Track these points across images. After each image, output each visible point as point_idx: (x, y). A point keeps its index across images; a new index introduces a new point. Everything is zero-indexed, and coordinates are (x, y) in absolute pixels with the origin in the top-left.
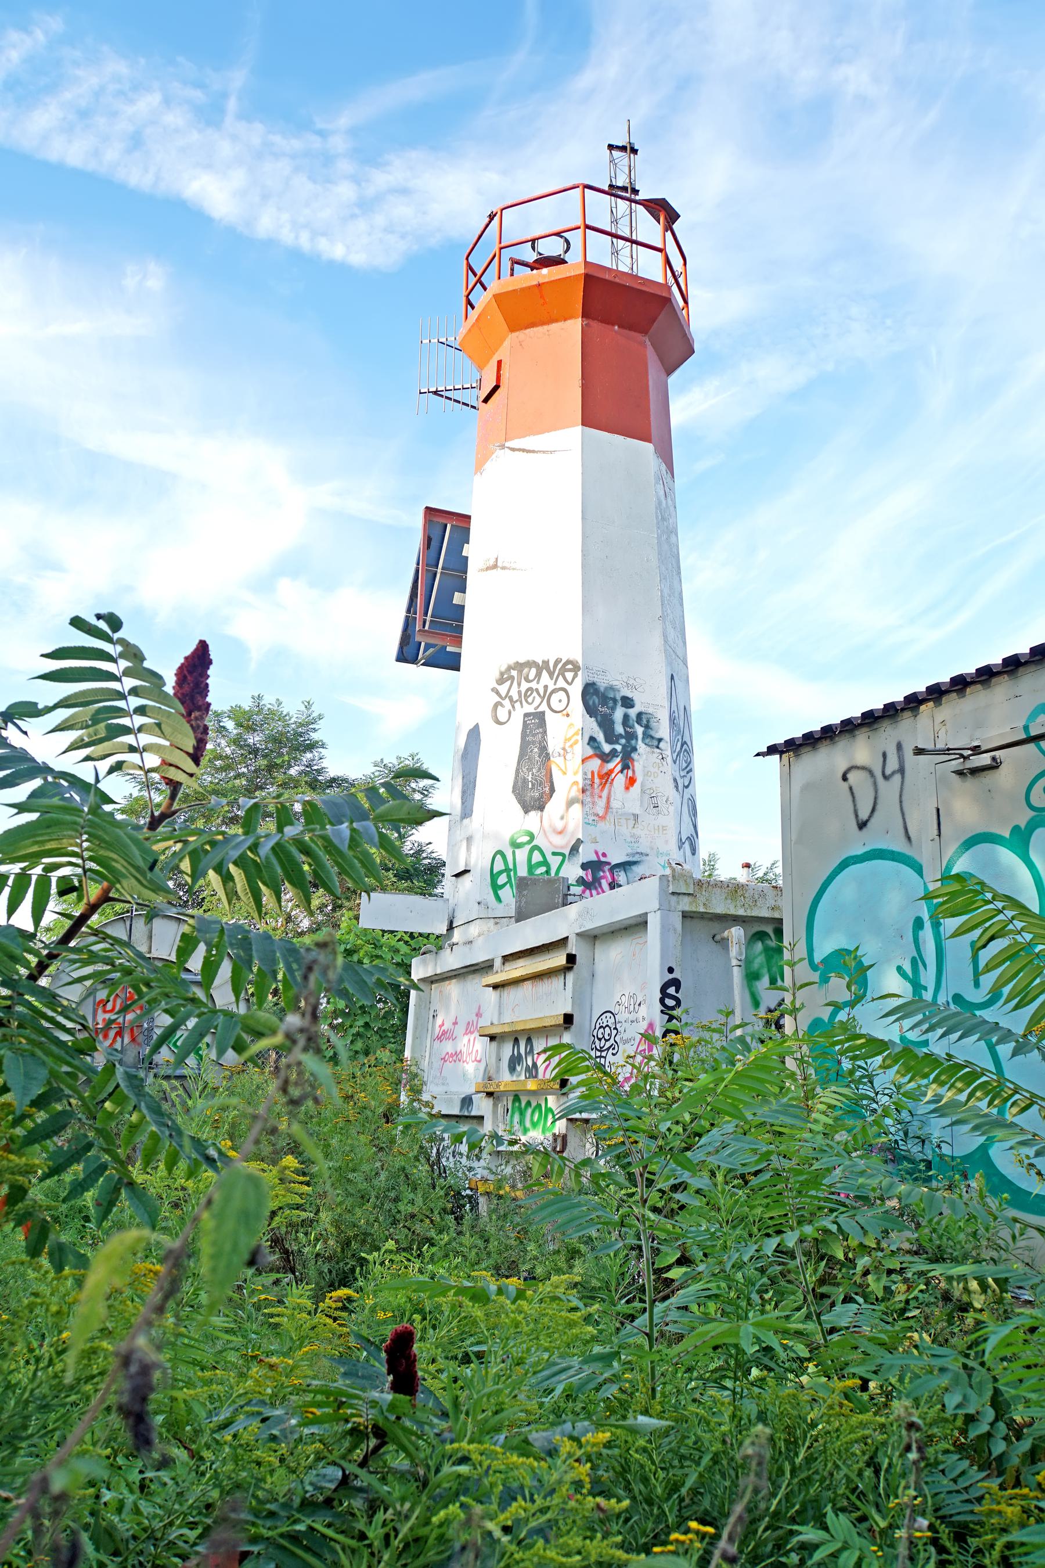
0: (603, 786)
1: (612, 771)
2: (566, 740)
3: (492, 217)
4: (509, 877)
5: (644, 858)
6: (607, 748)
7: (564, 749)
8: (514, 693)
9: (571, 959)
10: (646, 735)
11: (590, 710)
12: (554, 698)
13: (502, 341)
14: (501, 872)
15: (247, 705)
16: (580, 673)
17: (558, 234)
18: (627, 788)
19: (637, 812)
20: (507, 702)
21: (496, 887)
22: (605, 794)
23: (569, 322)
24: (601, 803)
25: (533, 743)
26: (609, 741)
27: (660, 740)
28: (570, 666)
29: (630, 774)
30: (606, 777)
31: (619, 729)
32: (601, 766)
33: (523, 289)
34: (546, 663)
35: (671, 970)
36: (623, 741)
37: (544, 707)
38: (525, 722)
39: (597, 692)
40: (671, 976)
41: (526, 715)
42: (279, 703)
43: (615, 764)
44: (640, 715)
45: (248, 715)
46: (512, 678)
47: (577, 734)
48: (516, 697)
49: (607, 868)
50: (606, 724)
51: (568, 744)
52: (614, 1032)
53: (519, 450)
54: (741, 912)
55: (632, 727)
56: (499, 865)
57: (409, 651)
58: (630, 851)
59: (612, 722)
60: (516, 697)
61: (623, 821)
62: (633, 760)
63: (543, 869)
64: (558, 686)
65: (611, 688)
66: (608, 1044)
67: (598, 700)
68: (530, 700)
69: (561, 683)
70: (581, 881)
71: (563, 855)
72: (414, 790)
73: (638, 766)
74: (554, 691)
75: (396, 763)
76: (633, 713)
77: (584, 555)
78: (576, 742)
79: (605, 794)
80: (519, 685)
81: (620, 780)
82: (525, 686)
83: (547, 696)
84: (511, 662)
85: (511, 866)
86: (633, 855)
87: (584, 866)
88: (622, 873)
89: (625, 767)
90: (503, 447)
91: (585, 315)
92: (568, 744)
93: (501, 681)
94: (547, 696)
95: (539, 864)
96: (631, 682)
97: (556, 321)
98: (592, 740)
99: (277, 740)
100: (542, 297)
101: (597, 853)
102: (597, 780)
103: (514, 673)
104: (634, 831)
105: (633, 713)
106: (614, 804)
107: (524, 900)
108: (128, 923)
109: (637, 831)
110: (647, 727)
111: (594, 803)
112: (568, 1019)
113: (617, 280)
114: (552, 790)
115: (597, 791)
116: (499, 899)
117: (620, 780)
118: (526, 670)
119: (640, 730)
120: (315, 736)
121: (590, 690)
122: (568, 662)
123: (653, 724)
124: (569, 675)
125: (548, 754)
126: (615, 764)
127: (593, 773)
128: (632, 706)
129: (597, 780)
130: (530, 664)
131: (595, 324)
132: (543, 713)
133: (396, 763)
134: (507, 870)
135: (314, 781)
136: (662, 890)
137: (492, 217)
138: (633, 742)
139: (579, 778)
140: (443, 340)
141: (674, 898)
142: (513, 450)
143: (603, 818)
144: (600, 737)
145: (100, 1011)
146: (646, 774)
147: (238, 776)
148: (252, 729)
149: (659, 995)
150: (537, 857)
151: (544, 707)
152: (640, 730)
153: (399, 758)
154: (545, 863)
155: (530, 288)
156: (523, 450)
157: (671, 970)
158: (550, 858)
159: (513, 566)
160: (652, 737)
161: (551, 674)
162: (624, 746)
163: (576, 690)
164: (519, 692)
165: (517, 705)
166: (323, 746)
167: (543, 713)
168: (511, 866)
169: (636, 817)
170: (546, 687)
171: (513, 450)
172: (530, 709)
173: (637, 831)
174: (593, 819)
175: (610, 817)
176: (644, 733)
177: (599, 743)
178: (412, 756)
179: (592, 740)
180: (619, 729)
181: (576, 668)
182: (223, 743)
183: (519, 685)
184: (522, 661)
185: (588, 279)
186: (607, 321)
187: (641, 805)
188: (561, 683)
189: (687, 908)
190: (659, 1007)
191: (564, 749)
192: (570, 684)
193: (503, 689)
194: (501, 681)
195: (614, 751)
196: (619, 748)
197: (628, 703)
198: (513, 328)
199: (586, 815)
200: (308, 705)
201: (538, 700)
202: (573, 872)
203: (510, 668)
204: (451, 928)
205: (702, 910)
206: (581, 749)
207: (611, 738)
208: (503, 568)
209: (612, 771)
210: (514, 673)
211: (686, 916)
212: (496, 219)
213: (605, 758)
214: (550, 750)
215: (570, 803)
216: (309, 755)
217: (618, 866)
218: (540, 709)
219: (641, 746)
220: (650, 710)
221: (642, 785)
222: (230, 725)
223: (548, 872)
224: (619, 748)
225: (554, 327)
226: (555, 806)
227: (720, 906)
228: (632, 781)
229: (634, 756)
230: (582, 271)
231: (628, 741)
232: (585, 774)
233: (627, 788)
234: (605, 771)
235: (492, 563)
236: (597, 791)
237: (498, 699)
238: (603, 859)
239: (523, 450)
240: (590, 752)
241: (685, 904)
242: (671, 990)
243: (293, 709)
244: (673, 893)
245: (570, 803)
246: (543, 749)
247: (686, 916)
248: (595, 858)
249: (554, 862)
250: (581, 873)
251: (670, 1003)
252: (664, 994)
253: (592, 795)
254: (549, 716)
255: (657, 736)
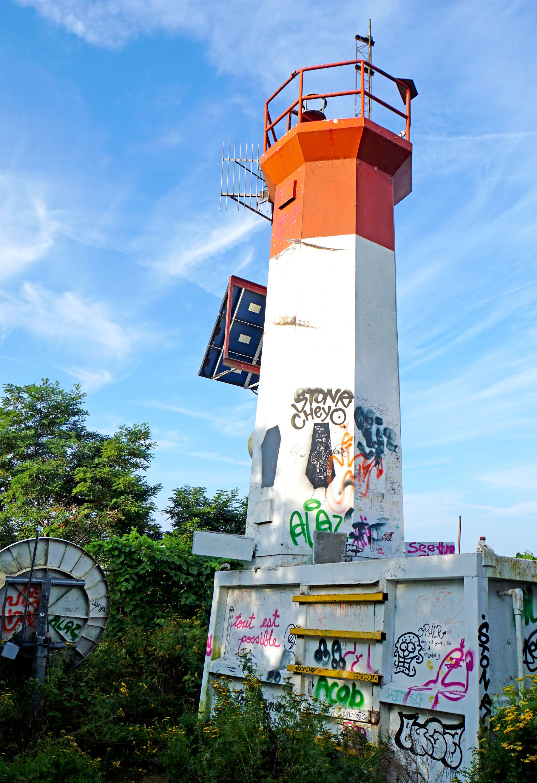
0: (365, 474)
1: (370, 465)
2: (344, 443)
3: (294, 75)
4: (303, 529)
5: (387, 521)
6: (368, 450)
7: (342, 449)
8: (307, 409)
9: (385, 596)
10: (389, 443)
11: (359, 425)
12: (336, 415)
13: (297, 167)
14: (297, 525)
15: (38, 383)
16: (353, 400)
17: (323, 98)
18: (378, 477)
19: (383, 492)
20: (302, 415)
21: (293, 535)
22: (366, 480)
23: (347, 160)
24: (364, 485)
25: (321, 443)
26: (369, 446)
27: (396, 447)
28: (346, 395)
29: (380, 468)
30: (367, 468)
31: (374, 438)
32: (364, 462)
33: (319, 132)
34: (330, 392)
35: (483, 617)
36: (376, 446)
37: (328, 420)
38: (315, 429)
39: (362, 413)
40: (484, 621)
41: (316, 424)
42: (57, 383)
43: (371, 461)
44: (385, 430)
45: (40, 390)
46: (306, 399)
47: (351, 440)
48: (308, 412)
49: (367, 527)
50: (367, 434)
51: (344, 446)
52: (418, 648)
53: (311, 245)
54: (518, 578)
55: (381, 437)
56: (296, 521)
57: (208, 370)
58: (379, 517)
59: (371, 434)
60: (308, 412)
61: (376, 498)
62: (381, 459)
63: (327, 526)
64: (338, 407)
65: (370, 411)
66: (411, 655)
67: (363, 418)
68: (319, 414)
69: (340, 405)
70: (352, 535)
71: (340, 517)
72: (142, 445)
73: (384, 462)
74: (336, 410)
75: (133, 428)
76: (382, 428)
77: (356, 322)
78: (350, 445)
79: (366, 480)
80: (311, 404)
81: (374, 471)
82: (315, 405)
83: (330, 413)
84: (305, 387)
85: (304, 522)
86: (381, 519)
87: (354, 526)
88: (375, 531)
89: (377, 463)
90: (299, 242)
91: (358, 157)
92: (344, 446)
93: (298, 400)
94: (330, 413)
95: (324, 522)
96: (381, 408)
97: (337, 158)
98: (360, 444)
99: (56, 407)
100: (331, 139)
101: (361, 517)
102: (362, 471)
103: (307, 396)
104: (382, 504)
105: (382, 428)
106: (371, 487)
107: (320, 547)
108: (32, 545)
109: (383, 504)
110: (389, 438)
111: (360, 485)
112: (384, 636)
113: (382, 134)
114: (334, 475)
115: (362, 478)
116: (295, 543)
117: (374, 471)
118: (316, 395)
119: (385, 439)
120: (80, 407)
121: (358, 412)
122: (345, 392)
123: (392, 436)
124: (346, 401)
125: (331, 451)
126: (371, 461)
127: (360, 466)
128: (381, 424)
129: (362, 471)
130: (320, 391)
131: (364, 164)
132: (328, 424)
133: (133, 428)
134: (302, 525)
135: (82, 436)
136: (479, 563)
137: (294, 75)
138: (382, 447)
139: (352, 469)
140: (238, 160)
141: (484, 569)
142: (307, 245)
143: (365, 495)
144: (364, 443)
145: (7, 604)
146: (389, 468)
147: (29, 428)
148: (42, 399)
149: (478, 634)
150: (322, 517)
151: (328, 420)
152: (385, 439)
153: (135, 425)
154: (328, 522)
155: (324, 131)
156: (314, 246)
157: (483, 617)
158: (332, 519)
159: (307, 324)
160: (392, 445)
161: (333, 400)
162: (377, 450)
163: (351, 411)
164: (311, 409)
165: (310, 417)
166: (87, 413)
167: (328, 424)
168: (304, 522)
169: (383, 495)
170: (330, 407)
171: (307, 245)
172: (319, 421)
173: (383, 504)
174: (360, 495)
175: (369, 495)
176: (388, 442)
177: (363, 447)
178: (144, 425)
179: (360, 444)
180: (374, 438)
181: (350, 397)
182: (20, 407)
183: (311, 404)
184: (312, 387)
185: (366, 129)
186: (372, 163)
187: (386, 488)
188: (340, 405)
189: (491, 576)
190: (477, 642)
191: (342, 449)
192: (346, 407)
193: (300, 406)
194: (298, 400)
195: (371, 452)
196: (374, 450)
197: (379, 421)
198: (308, 158)
199: (356, 493)
200: (78, 387)
201: (324, 415)
202: (347, 528)
203: (304, 392)
204: (254, 556)
205: (499, 577)
206: (352, 451)
207: (370, 444)
208: (300, 325)
209: (370, 465)
210: (307, 396)
211: (491, 580)
212: (298, 77)
213: (367, 456)
214: (332, 449)
215: (346, 484)
216: (76, 418)
217: (373, 526)
218: (325, 422)
219: (386, 450)
220: (391, 427)
221: (386, 475)
222: (25, 396)
223: (330, 528)
224: (374, 450)
225: (337, 162)
226: (336, 484)
227: (508, 575)
228: (380, 472)
229: (382, 456)
230: (362, 124)
231: (379, 446)
232: (355, 466)
233: (378, 477)
234: (366, 465)
235: (290, 320)
236: (362, 478)
237: (296, 412)
238: (365, 522)
239: (314, 246)
240: (359, 452)
241: (490, 573)
242: (484, 631)
243: (67, 388)
244: (484, 566)
245: (346, 484)
246: (327, 447)
247: (491, 580)
248: (360, 521)
249: (335, 522)
250: (353, 530)
251: (484, 639)
252: (481, 634)
253: (359, 480)
254: (332, 426)
255: (395, 444)
